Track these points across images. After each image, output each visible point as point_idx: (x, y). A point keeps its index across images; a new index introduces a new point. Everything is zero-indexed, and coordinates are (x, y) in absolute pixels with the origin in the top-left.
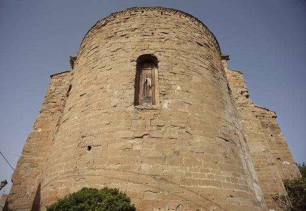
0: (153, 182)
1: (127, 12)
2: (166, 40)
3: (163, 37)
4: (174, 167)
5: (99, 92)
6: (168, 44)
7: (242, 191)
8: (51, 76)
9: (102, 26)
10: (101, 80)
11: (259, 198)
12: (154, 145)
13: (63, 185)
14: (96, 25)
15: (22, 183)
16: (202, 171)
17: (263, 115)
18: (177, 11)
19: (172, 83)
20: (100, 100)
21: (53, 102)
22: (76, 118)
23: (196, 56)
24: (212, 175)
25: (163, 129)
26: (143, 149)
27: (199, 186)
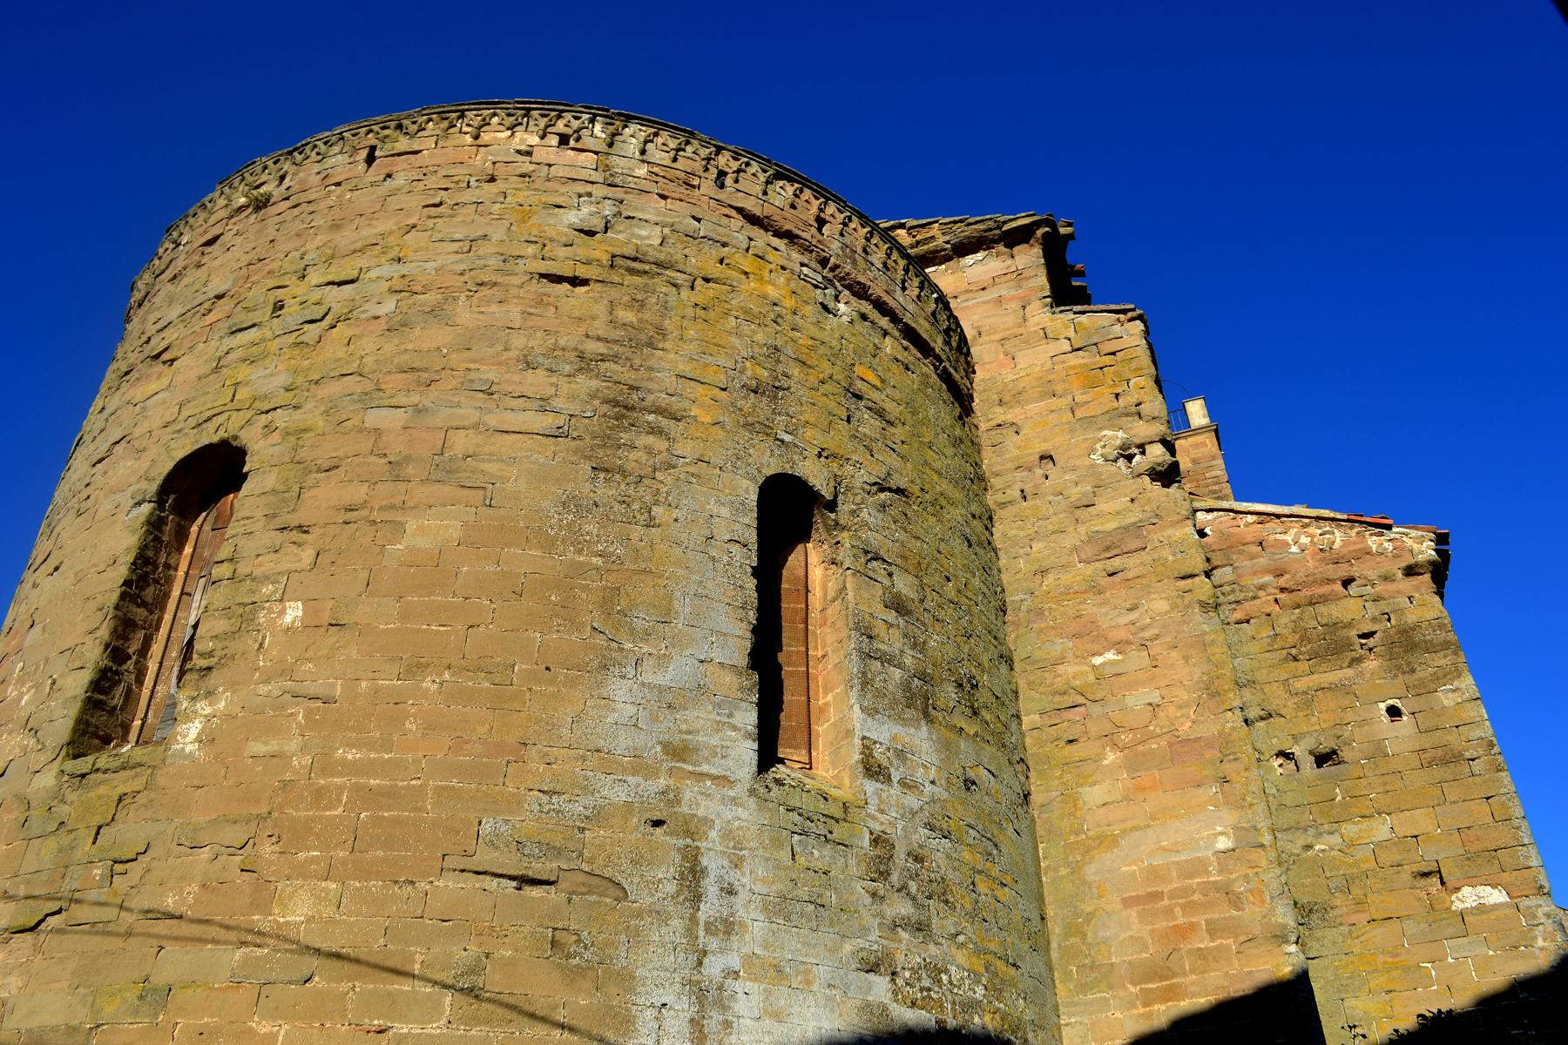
17: (1343, 571)
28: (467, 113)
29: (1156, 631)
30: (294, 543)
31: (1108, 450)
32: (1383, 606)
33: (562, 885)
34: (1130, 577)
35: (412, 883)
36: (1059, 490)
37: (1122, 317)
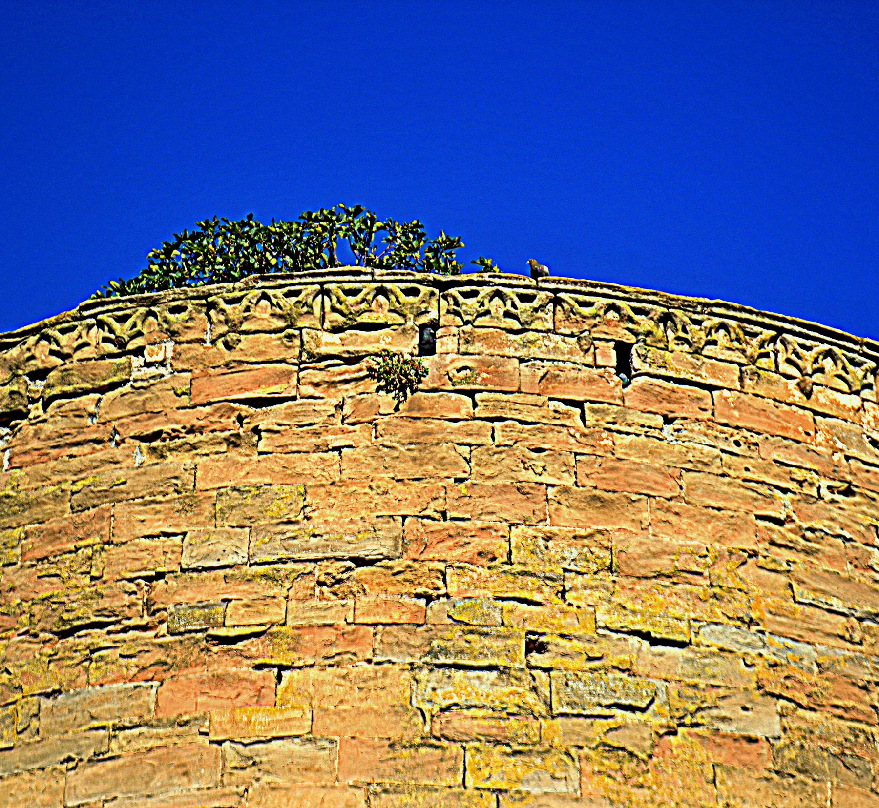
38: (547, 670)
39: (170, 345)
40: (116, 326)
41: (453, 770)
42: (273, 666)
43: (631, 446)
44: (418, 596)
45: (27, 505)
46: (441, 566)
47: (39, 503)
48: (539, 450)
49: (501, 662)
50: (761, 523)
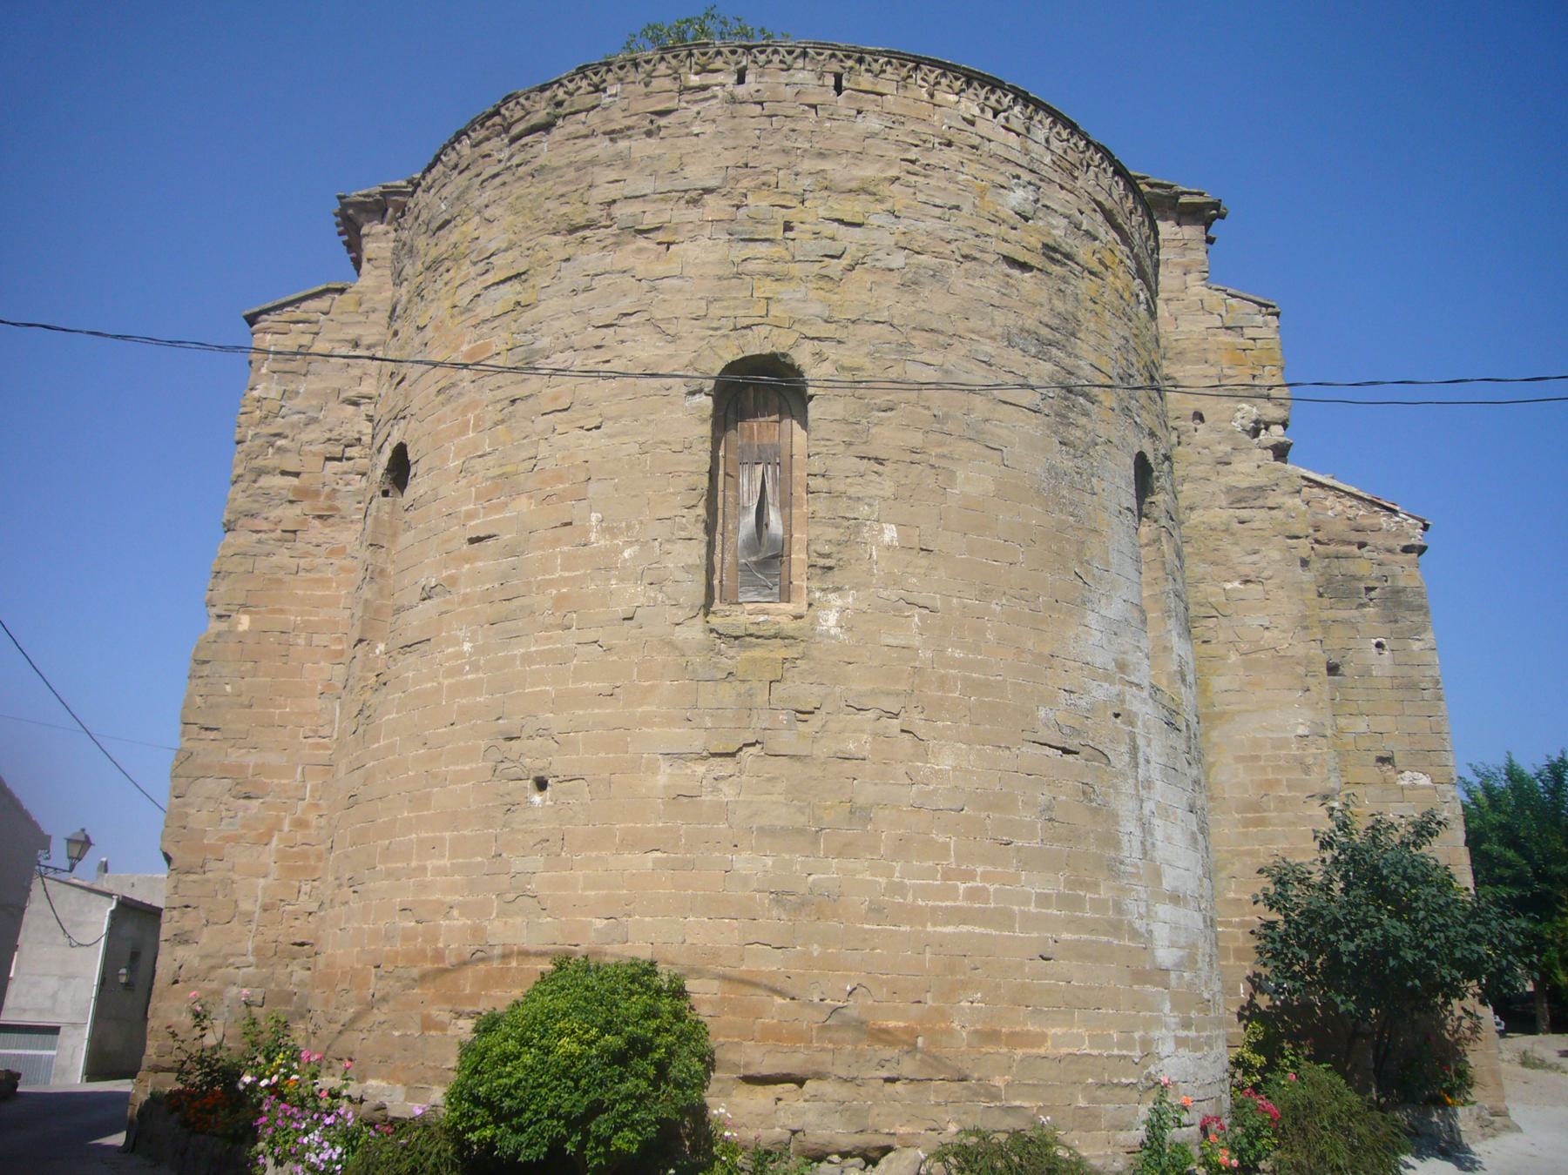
0: (774, 913)
1: (662, 68)
2: (852, 268)
3: (835, 248)
4: (851, 864)
5: (557, 542)
6: (856, 293)
7: (1094, 938)
8: (252, 320)
9: (532, 130)
10: (560, 478)
11: (1165, 955)
12: (781, 786)
13: (455, 913)
14: (497, 113)
15: (213, 865)
16: (946, 877)
17: (1360, 537)
18: (918, 62)
19: (864, 510)
20: (566, 581)
21: (246, 413)
22: (467, 647)
23: (987, 347)
24: (984, 889)
25: (815, 721)
26: (741, 798)
27: (930, 928)
28: (922, 66)
29: (1270, 573)
30: (876, 472)
31: (1245, 422)
32: (1384, 570)
33: (1082, 754)
34: (1255, 527)
35: (1009, 748)
36: (1207, 444)
37: (1264, 309)
38: (793, 240)
39: (619, 86)
40: (593, 77)
41: (746, 289)
42: (664, 243)
43: (839, 126)
44: (733, 206)
45: (554, 169)
46: (745, 191)
47: (560, 168)
48: (794, 130)
49: (771, 236)
50: (903, 163)
